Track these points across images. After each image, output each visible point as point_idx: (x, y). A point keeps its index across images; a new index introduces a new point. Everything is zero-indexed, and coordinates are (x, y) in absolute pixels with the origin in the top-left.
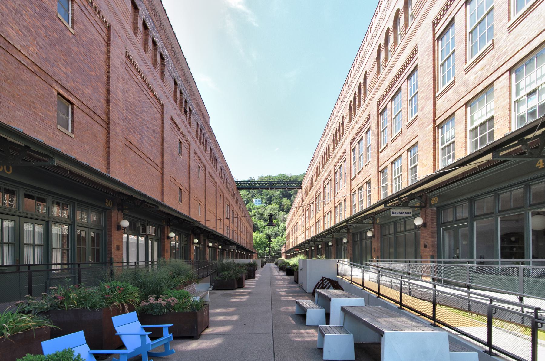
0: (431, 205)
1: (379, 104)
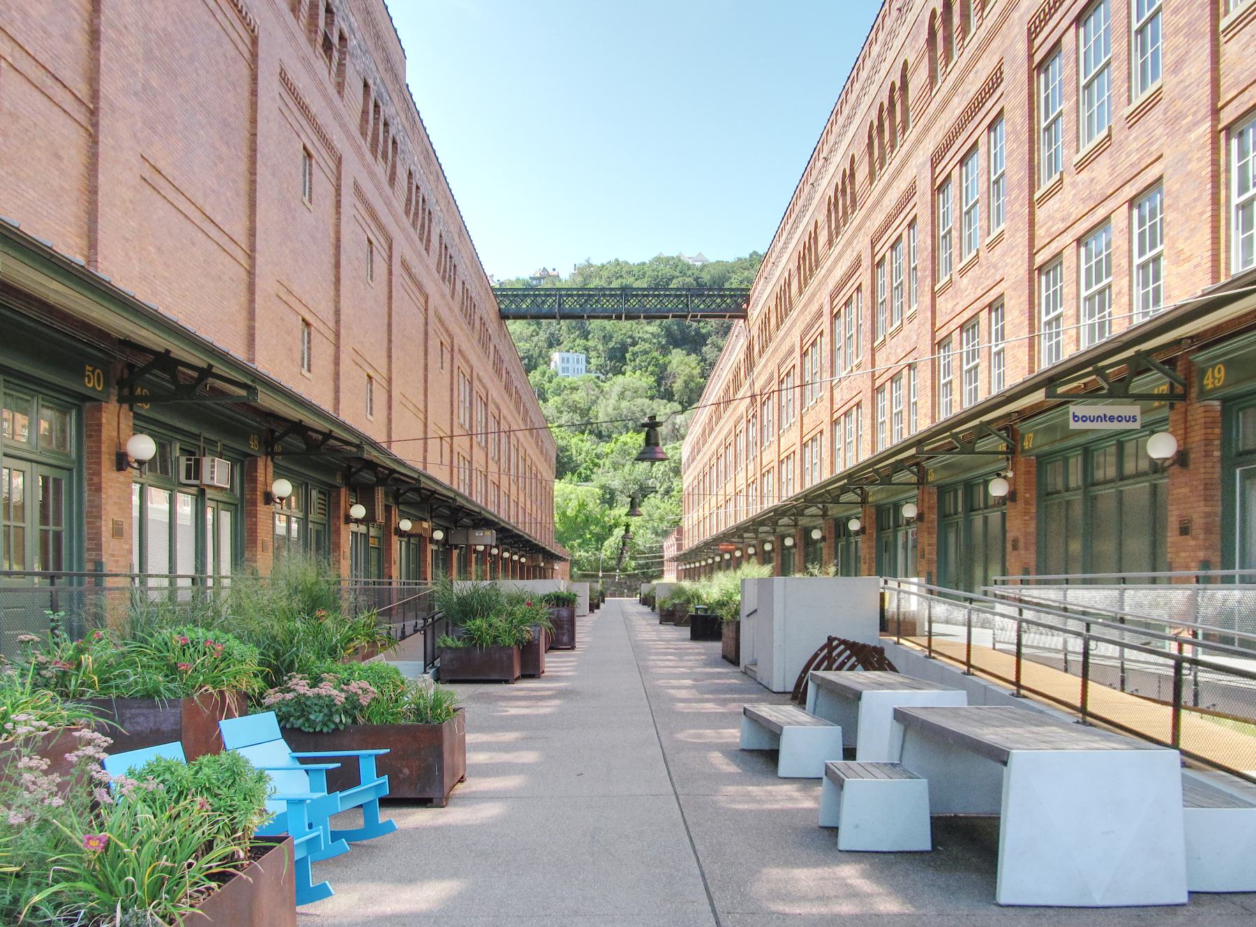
0: (1204, 394)
1: (1032, 34)
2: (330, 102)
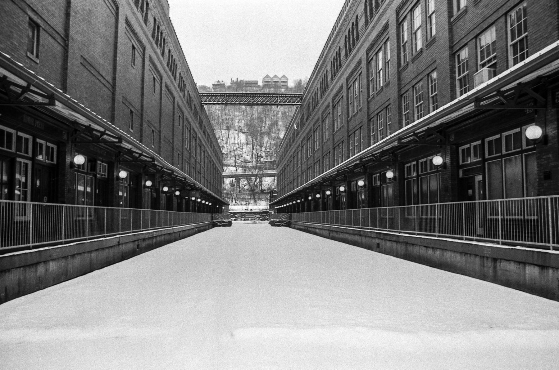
2: (141, 26)
